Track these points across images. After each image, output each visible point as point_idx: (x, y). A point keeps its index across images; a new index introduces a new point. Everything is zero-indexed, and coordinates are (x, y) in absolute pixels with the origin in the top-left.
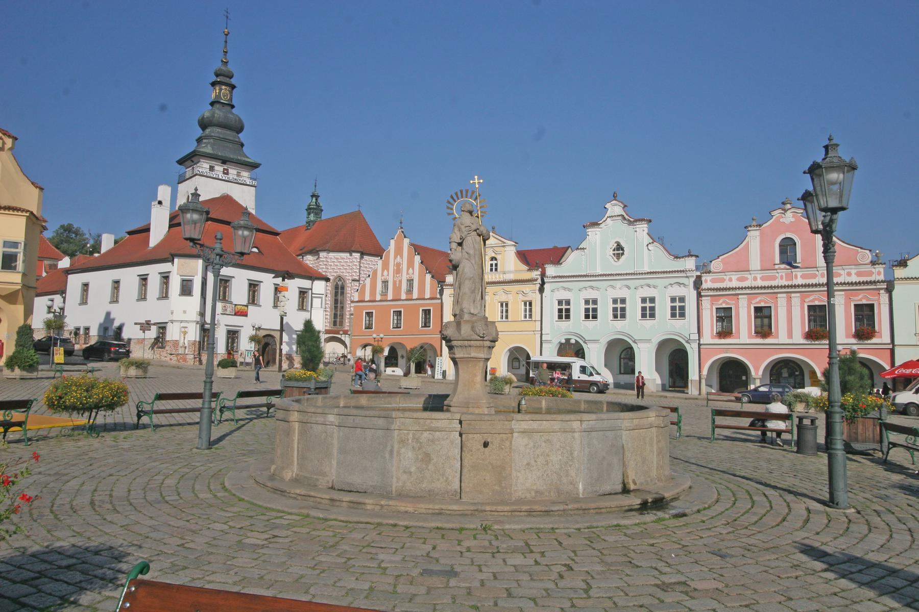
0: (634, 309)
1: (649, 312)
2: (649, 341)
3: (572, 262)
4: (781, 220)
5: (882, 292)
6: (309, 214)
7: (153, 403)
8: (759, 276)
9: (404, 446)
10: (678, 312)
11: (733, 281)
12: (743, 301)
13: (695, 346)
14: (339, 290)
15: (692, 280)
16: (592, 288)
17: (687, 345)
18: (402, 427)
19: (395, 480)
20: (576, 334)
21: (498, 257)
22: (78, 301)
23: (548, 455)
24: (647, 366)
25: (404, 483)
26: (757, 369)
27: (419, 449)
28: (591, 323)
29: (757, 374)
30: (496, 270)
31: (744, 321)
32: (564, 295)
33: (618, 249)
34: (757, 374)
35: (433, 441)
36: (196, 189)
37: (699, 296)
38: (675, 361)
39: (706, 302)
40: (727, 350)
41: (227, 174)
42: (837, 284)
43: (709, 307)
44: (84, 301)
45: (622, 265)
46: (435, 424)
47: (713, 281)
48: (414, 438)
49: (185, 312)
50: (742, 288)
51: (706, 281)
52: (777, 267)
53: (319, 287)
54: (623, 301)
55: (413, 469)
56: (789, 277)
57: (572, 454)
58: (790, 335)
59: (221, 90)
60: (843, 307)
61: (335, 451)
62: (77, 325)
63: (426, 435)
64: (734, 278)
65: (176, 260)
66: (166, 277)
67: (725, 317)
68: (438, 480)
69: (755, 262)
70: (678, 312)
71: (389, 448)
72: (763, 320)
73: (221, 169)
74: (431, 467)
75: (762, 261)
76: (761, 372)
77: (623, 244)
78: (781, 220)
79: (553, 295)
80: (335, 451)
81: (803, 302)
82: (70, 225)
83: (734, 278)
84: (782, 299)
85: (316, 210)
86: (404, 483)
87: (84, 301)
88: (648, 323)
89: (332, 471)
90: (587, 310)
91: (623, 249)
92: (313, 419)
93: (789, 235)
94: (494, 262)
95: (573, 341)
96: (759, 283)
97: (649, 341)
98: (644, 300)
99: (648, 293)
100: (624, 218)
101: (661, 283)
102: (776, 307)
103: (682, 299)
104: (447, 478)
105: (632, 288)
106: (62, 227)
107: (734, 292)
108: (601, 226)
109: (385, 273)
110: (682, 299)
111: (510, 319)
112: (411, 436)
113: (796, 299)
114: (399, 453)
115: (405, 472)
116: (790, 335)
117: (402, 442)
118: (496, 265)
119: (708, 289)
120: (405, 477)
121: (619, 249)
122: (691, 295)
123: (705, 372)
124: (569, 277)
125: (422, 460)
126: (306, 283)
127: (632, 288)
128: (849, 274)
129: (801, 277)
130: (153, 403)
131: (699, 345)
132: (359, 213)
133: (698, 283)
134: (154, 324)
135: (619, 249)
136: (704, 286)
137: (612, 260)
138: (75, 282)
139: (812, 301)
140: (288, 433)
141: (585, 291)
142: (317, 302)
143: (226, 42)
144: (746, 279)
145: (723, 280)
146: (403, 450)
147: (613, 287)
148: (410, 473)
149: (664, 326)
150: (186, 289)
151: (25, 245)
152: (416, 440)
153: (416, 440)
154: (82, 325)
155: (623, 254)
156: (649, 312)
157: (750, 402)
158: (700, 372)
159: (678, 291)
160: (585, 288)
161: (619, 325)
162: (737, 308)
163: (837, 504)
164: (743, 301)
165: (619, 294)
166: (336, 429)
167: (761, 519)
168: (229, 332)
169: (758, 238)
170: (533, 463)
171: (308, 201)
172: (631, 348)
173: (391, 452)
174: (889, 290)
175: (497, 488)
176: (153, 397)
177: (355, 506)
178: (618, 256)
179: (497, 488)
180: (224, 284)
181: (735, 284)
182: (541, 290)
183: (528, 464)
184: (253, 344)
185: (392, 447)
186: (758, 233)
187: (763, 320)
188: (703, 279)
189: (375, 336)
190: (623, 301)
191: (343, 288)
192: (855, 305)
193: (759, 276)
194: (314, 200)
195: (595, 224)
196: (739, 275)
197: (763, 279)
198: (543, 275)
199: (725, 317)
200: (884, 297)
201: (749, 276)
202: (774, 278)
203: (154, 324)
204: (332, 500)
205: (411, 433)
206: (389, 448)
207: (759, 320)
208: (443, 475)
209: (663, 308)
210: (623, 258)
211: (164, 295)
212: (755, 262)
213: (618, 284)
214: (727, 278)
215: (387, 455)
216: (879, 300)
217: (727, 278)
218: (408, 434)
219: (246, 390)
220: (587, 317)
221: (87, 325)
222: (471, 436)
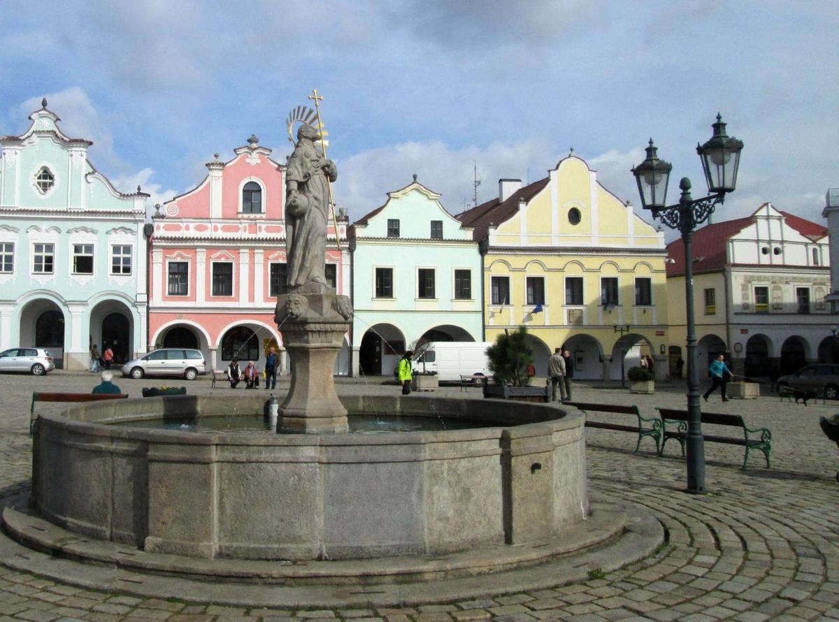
0: (65, 260)
1: (84, 265)
2: (84, 303)
4: (247, 160)
5: (344, 252)
8: (220, 226)
9: (437, 484)
10: (122, 267)
12: (201, 256)
13: (143, 310)
15: (141, 226)
16: (85, 229)
17: (133, 310)
18: (435, 455)
19: (426, 530)
24: (78, 337)
25: (440, 534)
27: (457, 483)
29: (214, 344)
31: (201, 277)
33: (45, 177)
34: (214, 344)
37: (150, 247)
38: (113, 326)
39: (157, 256)
40: (180, 315)
42: (157, 238)
43: (161, 260)
45: (51, 200)
46: (475, 447)
47: (167, 228)
48: (449, 469)
50: (201, 240)
51: (158, 228)
52: (240, 216)
54: (50, 247)
55: (451, 513)
56: (253, 228)
58: (252, 298)
60: (247, 266)
61: (320, 503)
63: (464, 463)
64: (192, 226)
67: (179, 274)
68: (480, 523)
69: (216, 210)
70: (122, 267)
71: (416, 487)
72: (223, 278)
74: (472, 507)
76: (218, 342)
77: (53, 171)
78: (247, 160)
80: (320, 503)
81: (266, 259)
83: (192, 226)
84: (244, 257)
86: (440, 534)
88: (84, 278)
89: (316, 530)
90: (116, 261)
91: (51, 178)
92: (265, 455)
93: (254, 179)
96: (220, 234)
97: (84, 303)
98: (116, 249)
100: (56, 136)
101: (102, 227)
102: (238, 264)
103: (127, 249)
104: (490, 519)
105: (23, 230)
108: (25, 143)
110: (127, 249)
112: (446, 466)
113: (259, 257)
114: (430, 493)
115: (440, 519)
116: (252, 298)
117: (435, 476)
119: (162, 239)
120: (440, 525)
121: (46, 178)
122: (139, 245)
123: (153, 343)
124: (53, 212)
125: (461, 499)
127: (64, 231)
131: (148, 308)
133: (148, 230)
135: (46, 178)
136: (156, 234)
137: (37, 191)
139: (219, 257)
140: (206, 483)
141: (113, 234)
145: (178, 228)
146: (436, 488)
147: (37, 228)
148: (448, 519)
149: (103, 284)
152: (453, 471)
153: (453, 471)
155: (51, 184)
156: (84, 265)
158: (148, 343)
159: (122, 239)
160: (115, 230)
161: (44, 280)
162: (195, 263)
163: (701, 489)
164: (201, 256)
165: (44, 239)
166: (318, 469)
169: (221, 180)
172: (61, 315)
173: (420, 493)
174: (351, 250)
175: (544, 522)
177: (407, 578)
178: (45, 187)
179: (544, 522)
181: (193, 233)
185: (421, 485)
186: (220, 173)
187: (223, 278)
190: (50, 247)
192: (214, 264)
193: (220, 226)
195: (14, 140)
196: (198, 223)
197: (225, 229)
199: (179, 274)
200: (346, 258)
201: (209, 225)
202: (236, 229)
204: (365, 576)
205: (445, 462)
207: (171, 276)
209: (103, 261)
210: (52, 190)
212: (216, 210)
213: (44, 225)
214: (183, 225)
215: (414, 498)
216: (340, 260)
217: (183, 225)
218: (442, 464)
220: (116, 269)
222: (520, 458)
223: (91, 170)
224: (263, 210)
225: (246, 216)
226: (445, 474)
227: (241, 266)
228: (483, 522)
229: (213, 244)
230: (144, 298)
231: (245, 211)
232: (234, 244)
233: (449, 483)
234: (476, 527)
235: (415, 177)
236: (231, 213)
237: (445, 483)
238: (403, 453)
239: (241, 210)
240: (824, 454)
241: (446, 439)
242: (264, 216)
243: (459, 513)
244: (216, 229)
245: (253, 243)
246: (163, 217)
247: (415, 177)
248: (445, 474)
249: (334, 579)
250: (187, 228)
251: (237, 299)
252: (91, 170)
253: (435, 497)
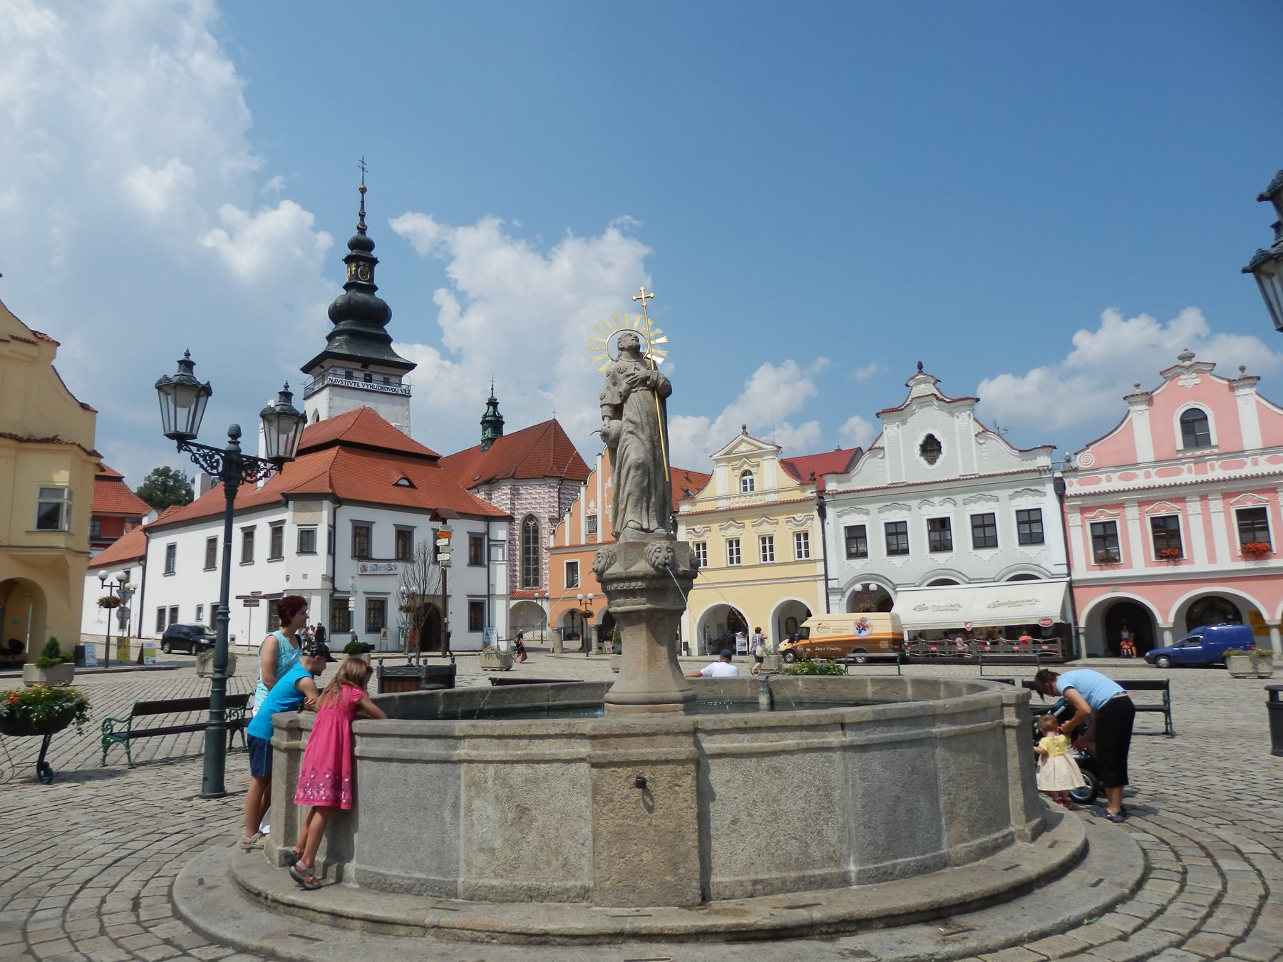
3: (868, 474)
6: (484, 429)
7: (130, 719)
9: (478, 795)
11: (1115, 483)
14: (531, 534)
20: (877, 577)
21: (753, 470)
22: (163, 570)
23: (775, 800)
26: (1165, 613)
27: (509, 799)
28: (898, 560)
29: (1165, 620)
30: (752, 488)
32: (854, 520)
34: (1165, 620)
35: (535, 782)
36: (188, 354)
39: (1074, 519)
41: (370, 381)
44: (169, 570)
45: (943, 468)
47: (1082, 484)
48: (497, 777)
49: (305, 576)
51: (1071, 484)
53: (500, 532)
55: (498, 844)
57: (827, 795)
58: (1212, 558)
59: (357, 267)
62: (161, 604)
65: (291, 503)
66: (277, 530)
68: (548, 863)
72: (1167, 538)
73: (362, 375)
74: (532, 837)
75: (1156, 448)
76: (1171, 619)
79: (838, 522)
82: (167, 470)
85: (493, 423)
87: (169, 570)
88: (986, 554)
94: (748, 478)
95: (873, 587)
96: (1156, 481)
99: (982, 508)
106: (157, 472)
107: (1115, 500)
109: (592, 504)
111: (811, 557)
114: (469, 810)
115: (482, 850)
116: (1212, 558)
118: (752, 481)
121: (931, 447)
122: (1049, 505)
126: (479, 527)
128: (1109, 479)
129: (1221, 466)
130: (130, 719)
132: (555, 422)
134: (264, 597)
135: (931, 447)
136: (1069, 491)
138: (157, 547)
142: (498, 553)
143: (362, 216)
144: (1135, 476)
146: (477, 803)
148: (492, 850)
150: (306, 544)
151: (70, 493)
152: (503, 781)
154: (168, 604)
157: (1170, 666)
159: (1027, 503)
165: (938, 513)
167: (1253, 922)
168: (370, 602)
170: (744, 817)
171: (484, 409)
173: (456, 806)
176: (130, 710)
180: (362, 533)
182: (822, 514)
183: (734, 822)
184: (404, 615)
185: (457, 797)
187: (1167, 538)
188: (1067, 481)
189: (580, 596)
191: (536, 530)
194: (491, 409)
198: (821, 493)
199: (1105, 542)
203: (264, 597)
206: (450, 800)
208: (557, 853)
211: (276, 553)
212: (1145, 452)
215: (448, 815)
219: (963, 667)
221: (173, 603)
223: (981, 429)
224: (1214, 441)
225: (1189, 454)
226: (490, 782)
227: (1129, 523)
228: (554, 863)
229: (1145, 497)
230: (1064, 570)
231: (1187, 445)
232: (1178, 494)
233: (496, 796)
234: (539, 869)
235: (920, 366)
236: (1168, 453)
237: (491, 796)
238: (432, 749)
239: (1180, 446)
240: (1249, 799)
241: (489, 732)
242: (1216, 451)
243: (513, 844)
244: (1148, 475)
245: (1203, 490)
246: (1076, 470)
247: (920, 366)
248: (490, 782)
249: (311, 913)
250: (1109, 479)
251: (1191, 562)
252: (981, 429)
253: (476, 814)
